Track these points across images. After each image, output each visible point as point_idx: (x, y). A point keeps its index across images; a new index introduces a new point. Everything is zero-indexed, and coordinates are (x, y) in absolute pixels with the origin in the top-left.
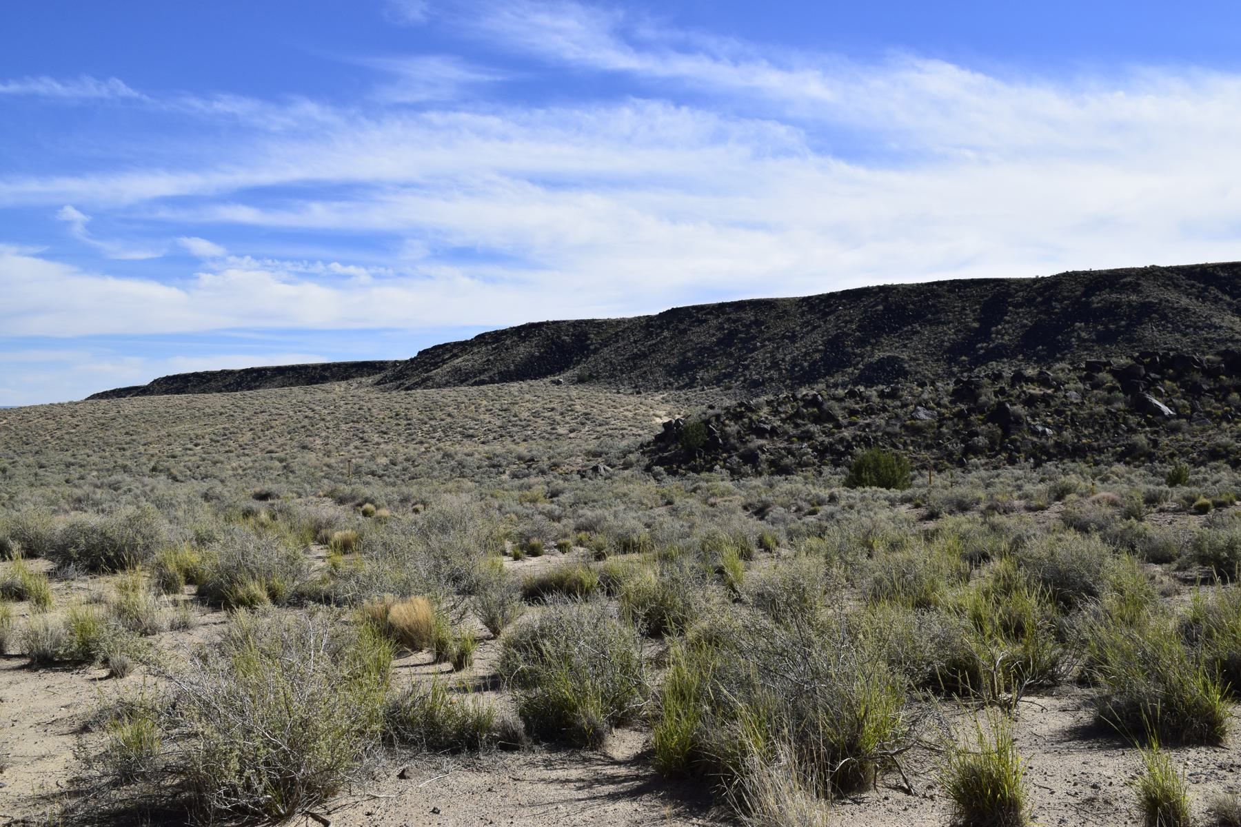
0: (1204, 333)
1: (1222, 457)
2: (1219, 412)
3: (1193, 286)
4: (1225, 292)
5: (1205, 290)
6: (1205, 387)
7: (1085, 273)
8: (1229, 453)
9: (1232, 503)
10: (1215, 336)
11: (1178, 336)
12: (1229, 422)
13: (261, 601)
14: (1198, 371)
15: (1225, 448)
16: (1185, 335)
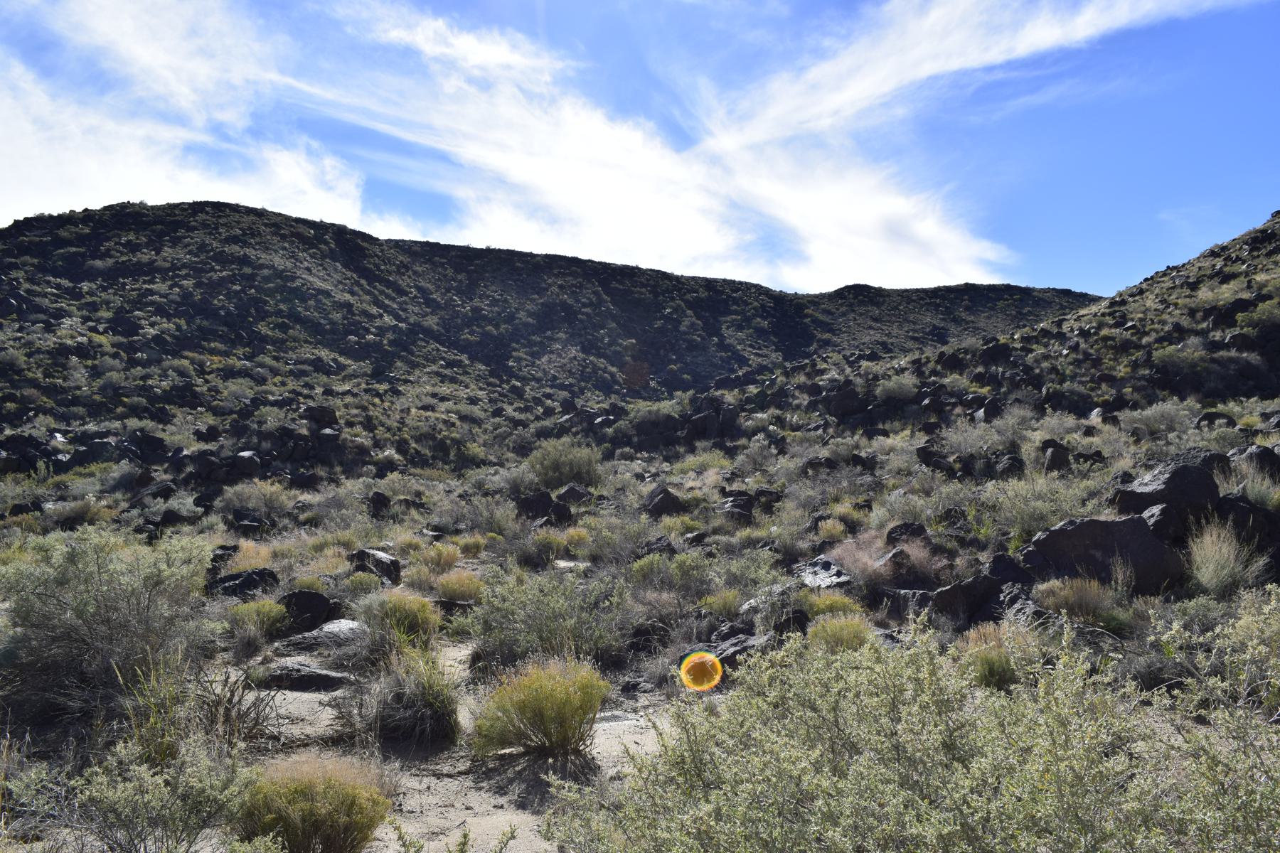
7: (600, 263)
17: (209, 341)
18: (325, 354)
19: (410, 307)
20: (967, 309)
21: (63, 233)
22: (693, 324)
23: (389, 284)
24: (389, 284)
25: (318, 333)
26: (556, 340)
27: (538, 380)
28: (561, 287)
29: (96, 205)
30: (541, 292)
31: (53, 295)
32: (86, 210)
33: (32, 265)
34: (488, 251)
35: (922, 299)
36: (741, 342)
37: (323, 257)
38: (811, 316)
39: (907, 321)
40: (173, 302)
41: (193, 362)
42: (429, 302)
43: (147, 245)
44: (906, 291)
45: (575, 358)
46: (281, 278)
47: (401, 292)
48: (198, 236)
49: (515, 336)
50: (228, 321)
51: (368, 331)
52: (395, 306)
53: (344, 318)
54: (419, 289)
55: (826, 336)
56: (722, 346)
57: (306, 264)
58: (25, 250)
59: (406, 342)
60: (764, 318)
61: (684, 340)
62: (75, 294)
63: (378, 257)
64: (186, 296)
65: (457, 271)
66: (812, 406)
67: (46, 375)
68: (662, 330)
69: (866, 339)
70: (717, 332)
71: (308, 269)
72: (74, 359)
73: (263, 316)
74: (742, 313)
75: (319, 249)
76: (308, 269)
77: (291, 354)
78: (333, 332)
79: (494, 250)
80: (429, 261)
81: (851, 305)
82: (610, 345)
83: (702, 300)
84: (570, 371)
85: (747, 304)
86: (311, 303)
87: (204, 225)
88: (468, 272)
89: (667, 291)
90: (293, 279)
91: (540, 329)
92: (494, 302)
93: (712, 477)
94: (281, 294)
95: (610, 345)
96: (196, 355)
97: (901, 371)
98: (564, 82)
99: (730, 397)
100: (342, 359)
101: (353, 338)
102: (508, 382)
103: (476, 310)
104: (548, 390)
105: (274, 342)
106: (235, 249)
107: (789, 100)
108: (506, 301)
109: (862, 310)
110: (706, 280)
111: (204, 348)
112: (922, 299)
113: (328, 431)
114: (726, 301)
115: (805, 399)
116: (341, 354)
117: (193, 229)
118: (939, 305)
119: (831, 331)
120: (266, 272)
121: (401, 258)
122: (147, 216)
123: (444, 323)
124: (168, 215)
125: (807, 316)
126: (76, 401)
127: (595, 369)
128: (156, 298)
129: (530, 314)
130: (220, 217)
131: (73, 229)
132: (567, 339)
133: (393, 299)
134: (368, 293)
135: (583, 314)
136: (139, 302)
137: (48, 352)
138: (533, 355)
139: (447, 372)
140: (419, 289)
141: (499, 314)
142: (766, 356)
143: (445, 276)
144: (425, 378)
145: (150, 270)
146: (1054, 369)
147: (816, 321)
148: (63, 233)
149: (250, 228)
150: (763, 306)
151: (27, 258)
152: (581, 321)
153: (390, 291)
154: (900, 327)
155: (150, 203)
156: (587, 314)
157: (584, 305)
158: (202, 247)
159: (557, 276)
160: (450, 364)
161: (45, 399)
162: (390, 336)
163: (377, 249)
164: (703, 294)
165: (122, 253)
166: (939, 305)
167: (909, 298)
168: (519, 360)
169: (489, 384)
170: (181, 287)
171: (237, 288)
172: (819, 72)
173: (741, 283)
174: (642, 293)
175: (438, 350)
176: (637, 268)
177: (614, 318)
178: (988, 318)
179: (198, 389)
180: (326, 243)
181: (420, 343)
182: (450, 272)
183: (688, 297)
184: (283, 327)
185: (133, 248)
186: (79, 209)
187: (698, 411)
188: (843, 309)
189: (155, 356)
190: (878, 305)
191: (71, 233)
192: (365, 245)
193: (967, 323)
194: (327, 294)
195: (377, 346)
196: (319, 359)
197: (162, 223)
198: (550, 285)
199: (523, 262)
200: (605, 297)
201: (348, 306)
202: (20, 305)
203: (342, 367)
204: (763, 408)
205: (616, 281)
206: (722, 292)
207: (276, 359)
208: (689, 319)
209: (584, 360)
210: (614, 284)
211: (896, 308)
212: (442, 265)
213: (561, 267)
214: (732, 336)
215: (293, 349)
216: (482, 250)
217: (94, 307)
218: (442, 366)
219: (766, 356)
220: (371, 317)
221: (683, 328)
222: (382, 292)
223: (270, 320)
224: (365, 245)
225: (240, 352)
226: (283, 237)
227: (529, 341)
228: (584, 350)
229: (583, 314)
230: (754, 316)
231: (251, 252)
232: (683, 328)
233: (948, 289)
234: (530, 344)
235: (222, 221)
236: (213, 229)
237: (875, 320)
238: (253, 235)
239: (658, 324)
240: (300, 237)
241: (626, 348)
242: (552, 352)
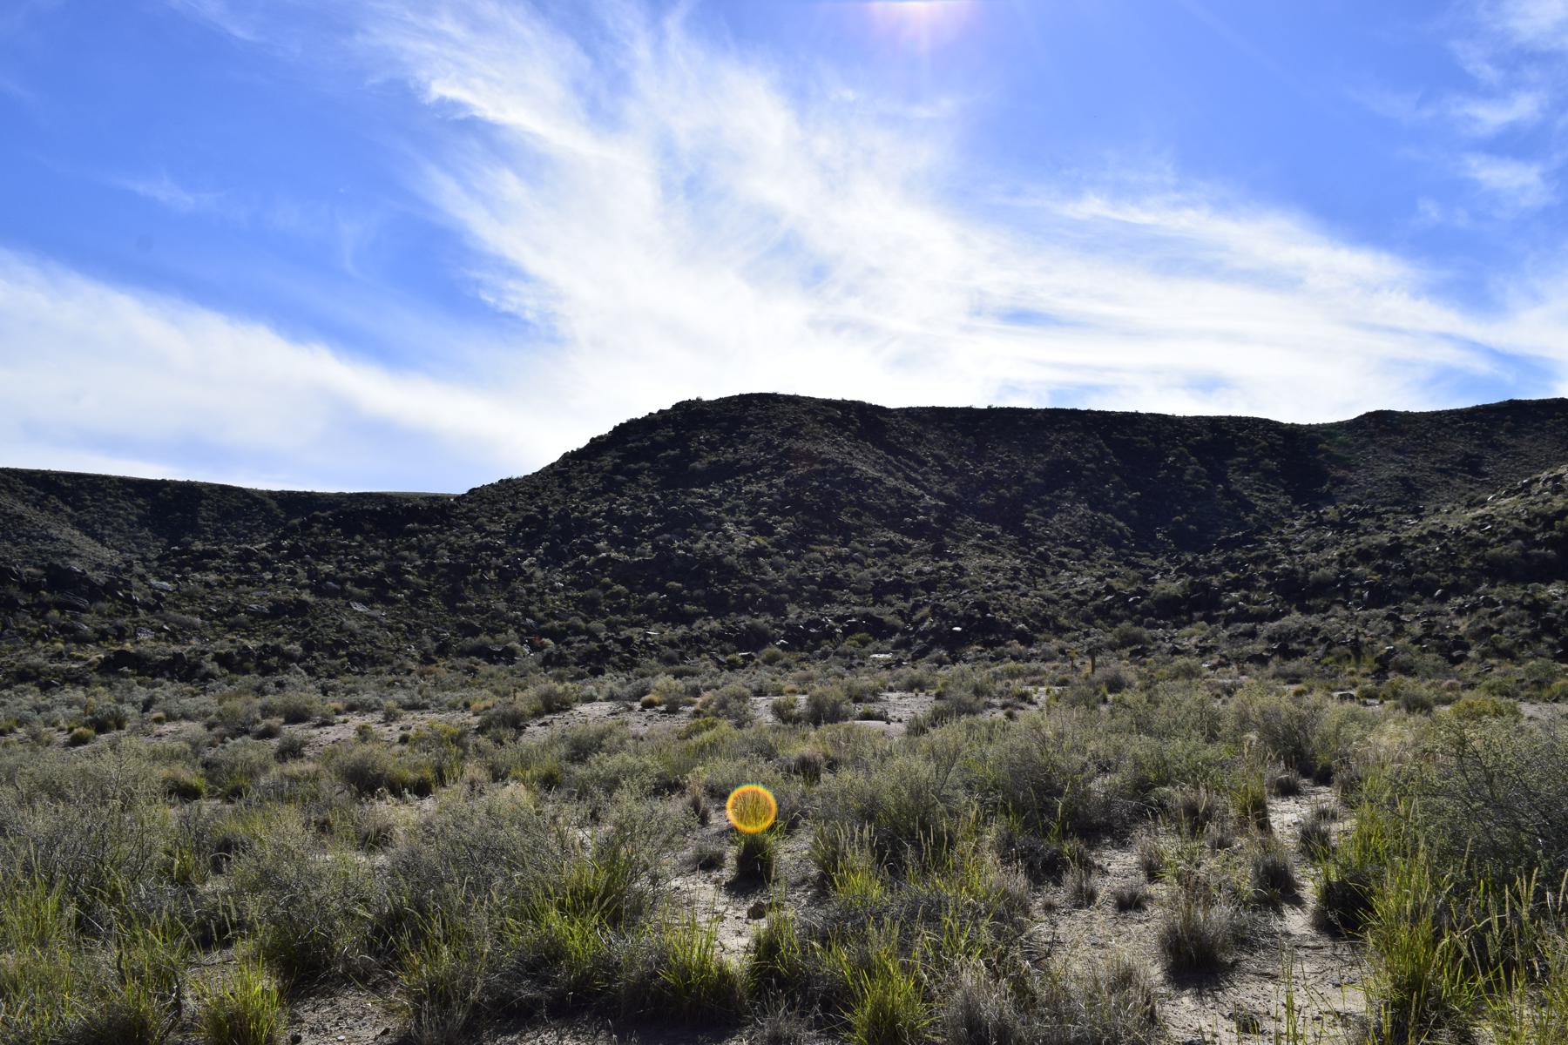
0: (39, 545)
1: (32, 679)
2: (35, 630)
3: (31, 492)
4: (66, 503)
5: (45, 498)
6: (22, 602)
7: (1099, 412)
8: (39, 674)
9: (12, 730)
10: (50, 548)
11: (7, 544)
12: (44, 640)
13: (1298, 902)
14: (15, 584)
15: (36, 668)
16: (16, 544)
20: (1509, 431)
22: (1197, 471)
26: (1066, 498)
27: (1053, 540)
28: (1064, 443)
30: (1045, 449)
34: (990, 410)
35: (1456, 422)
36: (1248, 486)
39: (1435, 450)
42: (946, 470)
54: (935, 457)
55: (1341, 473)
56: (1228, 493)
60: (1272, 458)
66: (1268, 588)
69: (1385, 475)
71: (850, 453)
73: (841, 507)
77: (869, 539)
81: (1371, 435)
82: (1116, 499)
85: (1253, 443)
93: (1194, 640)
95: (1116, 499)
97: (1329, 562)
99: (1215, 581)
101: (908, 520)
102: (1034, 548)
103: (988, 474)
104: (1063, 549)
105: (856, 529)
115: (1264, 583)
119: (1348, 467)
125: (1321, 451)
127: (1104, 524)
129: (1038, 474)
133: (916, 471)
138: (1045, 514)
139: (984, 543)
140: (935, 457)
142: (1274, 500)
144: (970, 551)
146: (1423, 563)
147: (1330, 456)
150: (1272, 445)
154: (1426, 458)
156: (1091, 470)
157: (1088, 461)
159: (1058, 431)
160: (986, 536)
164: (1207, 436)
166: (1474, 429)
168: (1033, 520)
169: (1020, 552)
178: (1534, 440)
180: (853, 423)
182: (958, 437)
183: (1191, 441)
184: (857, 515)
187: (1195, 592)
188: (1362, 440)
190: (1402, 433)
193: (1507, 447)
194: (879, 481)
195: (925, 524)
203: (909, 547)
204: (1236, 590)
210: (1115, 435)
212: (950, 429)
214: (1240, 481)
219: (1274, 500)
220: (917, 498)
221: (1187, 478)
222: (907, 465)
228: (1092, 507)
231: (798, 445)
232: (1187, 478)
234: (1041, 504)
235: (771, 413)
237: (1398, 451)
241: (1130, 501)
242: (1061, 511)
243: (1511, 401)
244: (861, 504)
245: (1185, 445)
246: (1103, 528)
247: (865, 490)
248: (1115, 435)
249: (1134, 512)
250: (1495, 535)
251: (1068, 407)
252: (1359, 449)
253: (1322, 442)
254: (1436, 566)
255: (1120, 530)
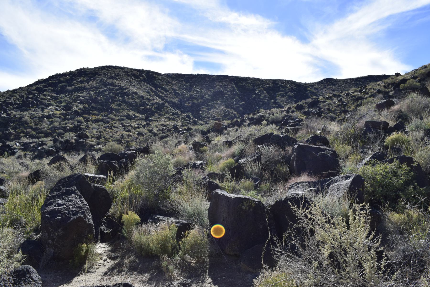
7: (235, 77)
17: (93, 111)
18: (131, 113)
19: (169, 96)
21: (62, 79)
23: (162, 88)
24: (162, 88)
25: (131, 107)
26: (217, 104)
27: (209, 118)
28: (221, 86)
29: (73, 69)
31: (49, 99)
32: (71, 71)
33: (51, 90)
35: (352, 82)
37: (141, 81)
38: (310, 90)
40: (86, 99)
41: (84, 118)
43: (86, 81)
44: (346, 79)
45: (222, 110)
46: (121, 89)
47: (166, 91)
48: (101, 77)
49: (203, 104)
50: (102, 104)
51: (148, 105)
52: (164, 96)
53: (140, 101)
54: (173, 89)
57: (134, 84)
58: (50, 85)
59: (160, 108)
60: (292, 92)
61: (261, 102)
62: (56, 98)
63: (160, 79)
64: (91, 97)
65: (187, 83)
67: (36, 124)
68: (254, 99)
70: (274, 98)
72: (46, 119)
74: (285, 91)
75: (140, 79)
76: (134, 86)
78: (136, 106)
79: (199, 75)
80: (178, 80)
81: (325, 86)
83: (270, 87)
84: (220, 114)
85: (286, 87)
86: (130, 97)
87: (104, 73)
88: (190, 83)
89: (258, 85)
90: (126, 89)
91: (212, 100)
92: (198, 92)
94: (121, 94)
95: (235, 104)
96: (87, 116)
98: (270, 28)
100: (136, 114)
101: (142, 107)
103: (191, 95)
106: (110, 81)
107: (339, 27)
108: (202, 92)
109: (328, 87)
110: (273, 80)
111: (91, 113)
112: (352, 82)
113: (82, 140)
114: (279, 87)
116: (138, 112)
117: (100, 75)
118: (358, 84)
120: (117, 87)
121: (168, 79)
122: (88, 72)
123: (180, 101)
124: (94, 71)
125: (308, 91)
126: (41, 133)
127: (229, 113)
128: (81, 98)
129: (209, 96)
130: (109, 70)
131: (65, 77)
132: (221, 103)
133: (163, 93)
134: (154, 92)
135: (227, 94)
136: (76, 100)
137: (38, 118)
140: (173, 89)
141: (199, 96)
143: (182, 84)
145: (82, 89)
146: (329, 109)
148: (62, 79)
149: (118, 73)
150: (292, 88)
151: (50, 88)
152: (226, 97)
153: (162, 91)
155: (90, 68)
156: (228, 94)
157: (228, 92)
158: (101, 81)
159: (220, 82)
160: (174, 114)
161: (33, 132)
162: (155, 106)
163: (160, 77)
164: (271, 85)
165: (78, 84)
166: (358, 84)
167: (347, 82)
169: (185, 120)
170: (90, 94)
171: (107, 93)
172: (351, 17)
173: (285, 80)
174: (248, 86)
175: (171, 110)
176: (249, 78)
177: (238, 95)
179: (82, 127)
181: (165, 108)
182: (184, 83)
183: (265, 86)
185: (82, 82)
186: (68, 71)
189: (73, 117)
190: (334, 85)
191: (64, 79)
192: (156, 76)
194: (136, 93)
195: (150, 110)
196: (129, 115)
197: (92, 74)
198: (217, 85)
199: (209, 78)
200: (236, 88)
201: (142, 97)
202: (37, 103)
203: (136, 117)
205: (240, 82)
206: (278, 84)
207: (115, 115)
208: (265, 93)
209: (226, 110)
210: (240, 84)
211: (341, 86)
212: (182, 81)
213: (221, 79)
215: (121, 112)
216: (196, 75)
217: (60, 102)
218: (171, 115)
220: (150, 100)
222: (159, 91)
223: (116, 103)
224: (156, 76)
225: (103, 114)
226: (128, 76)
227: (208, 105)
228: (227, 107)
229: (227, 94)
230: (289, 92)
232: (261, 97)
233: (362, 78)
236: (105, 74)
238: (118, 76)
239: (253, 96)
240: (134, 75)
241: (241, 105)
242: (215, 108)
243: (369, 76)
244: (124, 101)
245: (263, 88)
246: (229, 114)
247: (128, 96)
248: (240, 84)
249: (241, 109)
250: (368, 94)
251: (225, 75)
252: (320, 90)
253: (309, 88)
254: (335, 110)
255: (235, 115)
